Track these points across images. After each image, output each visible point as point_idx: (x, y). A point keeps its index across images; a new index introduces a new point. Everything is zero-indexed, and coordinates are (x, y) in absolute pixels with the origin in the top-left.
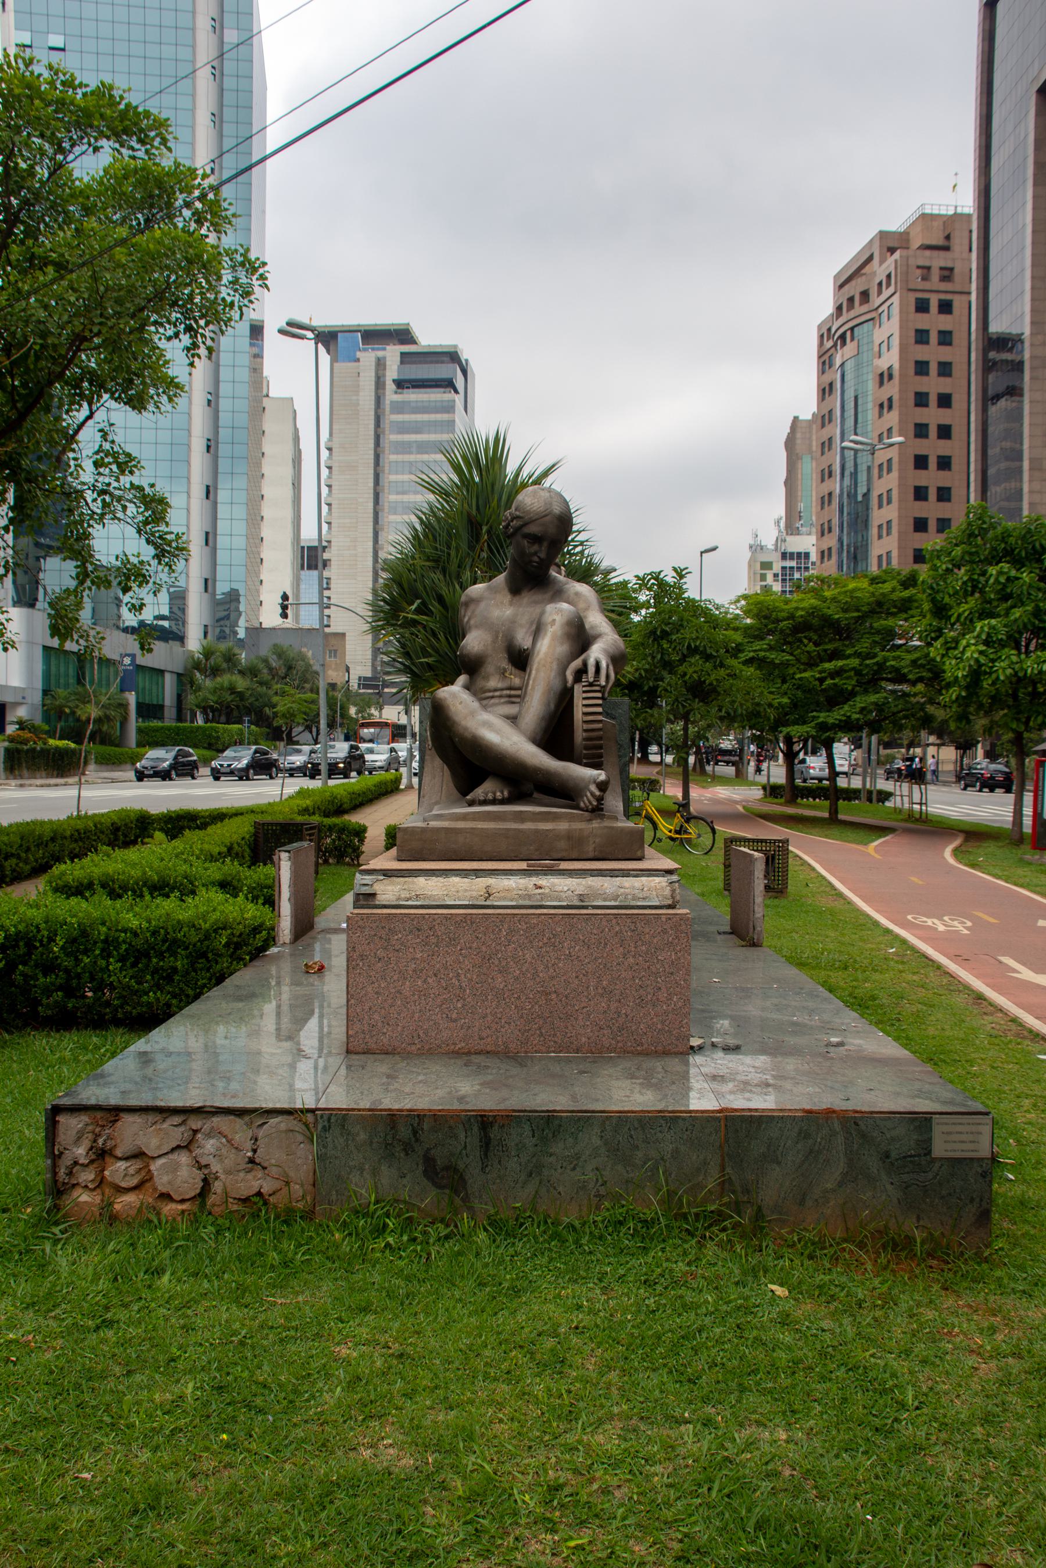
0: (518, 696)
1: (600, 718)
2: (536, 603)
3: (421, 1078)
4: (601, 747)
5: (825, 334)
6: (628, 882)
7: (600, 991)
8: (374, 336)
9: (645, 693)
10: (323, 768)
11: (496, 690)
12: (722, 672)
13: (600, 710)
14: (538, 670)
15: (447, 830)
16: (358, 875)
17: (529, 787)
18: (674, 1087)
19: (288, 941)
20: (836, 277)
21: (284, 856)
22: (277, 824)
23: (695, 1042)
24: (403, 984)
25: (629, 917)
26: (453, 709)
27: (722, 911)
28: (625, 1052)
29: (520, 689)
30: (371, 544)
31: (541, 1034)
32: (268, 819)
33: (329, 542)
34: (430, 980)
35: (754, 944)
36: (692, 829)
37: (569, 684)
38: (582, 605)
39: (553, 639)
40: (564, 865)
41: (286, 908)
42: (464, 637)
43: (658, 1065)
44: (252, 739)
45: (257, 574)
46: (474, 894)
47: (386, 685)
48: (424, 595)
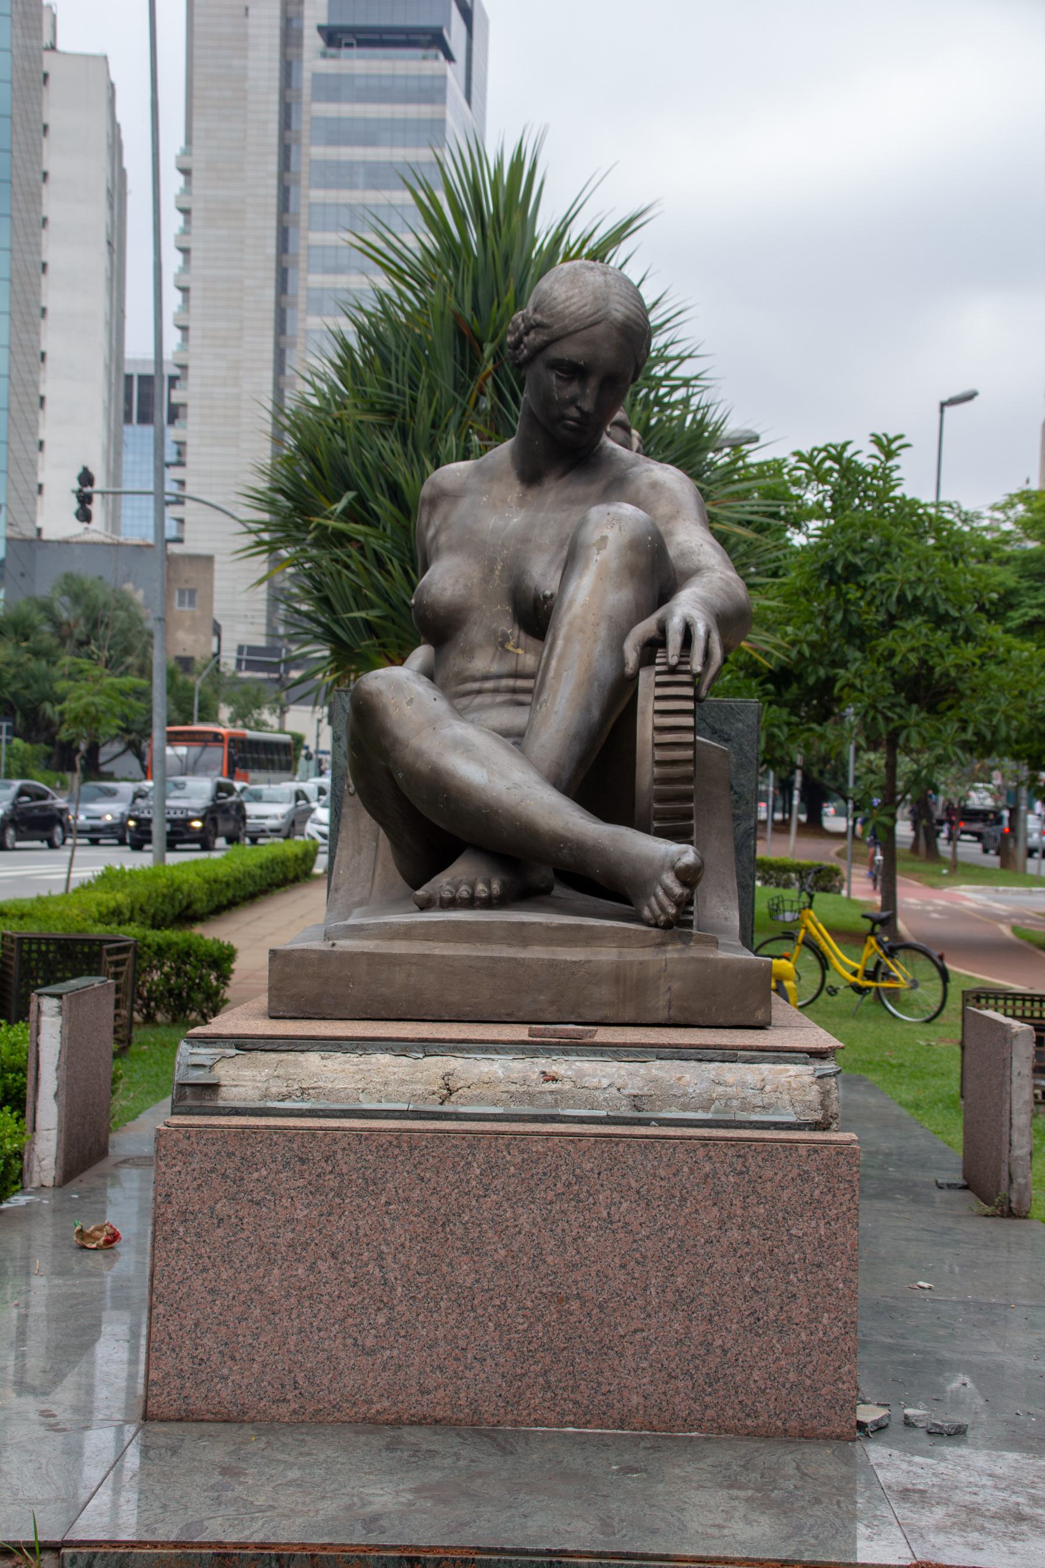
0: (528, 691)
1: (689, 737)
2: (572, 502)
3: (293, 1474)
4: (688, 797)
6: (733, 1073)
7: (670, 1297)
9: (811, 691)
10: (158, 830)
11: (486, 678)
12: (969, 651)
13: (689, 721)
14: (568, 640)
15: (371, 957)
16: (184, 1047)
17: (543, 874)
18: (818, 1510)
19: (49, 1182)
21: (49, 1005)
22: (48, 941)
23: (868, 1414)
24: (267, 1273)
25: (733, 1144)
26: (394, 713)
27: (945, 1140)
28: (722, 1430)
30: (269, 375)
31: (547, 1386)
32: (32, 929)
33: (184, 367)
34: (322, 1266)
35: (1011, 1212)
36: (900, 971)
37: (629, 669)
38: (663, 509)
39: (600, 577)
40: (603, 1035)
41: (48, 1112)
42: (426, 568)
43: (787, 1460)
44: (15, 765)
45: (33, 428)
46: (420, 1088)
47: (292, 662)
48: (363, 484)
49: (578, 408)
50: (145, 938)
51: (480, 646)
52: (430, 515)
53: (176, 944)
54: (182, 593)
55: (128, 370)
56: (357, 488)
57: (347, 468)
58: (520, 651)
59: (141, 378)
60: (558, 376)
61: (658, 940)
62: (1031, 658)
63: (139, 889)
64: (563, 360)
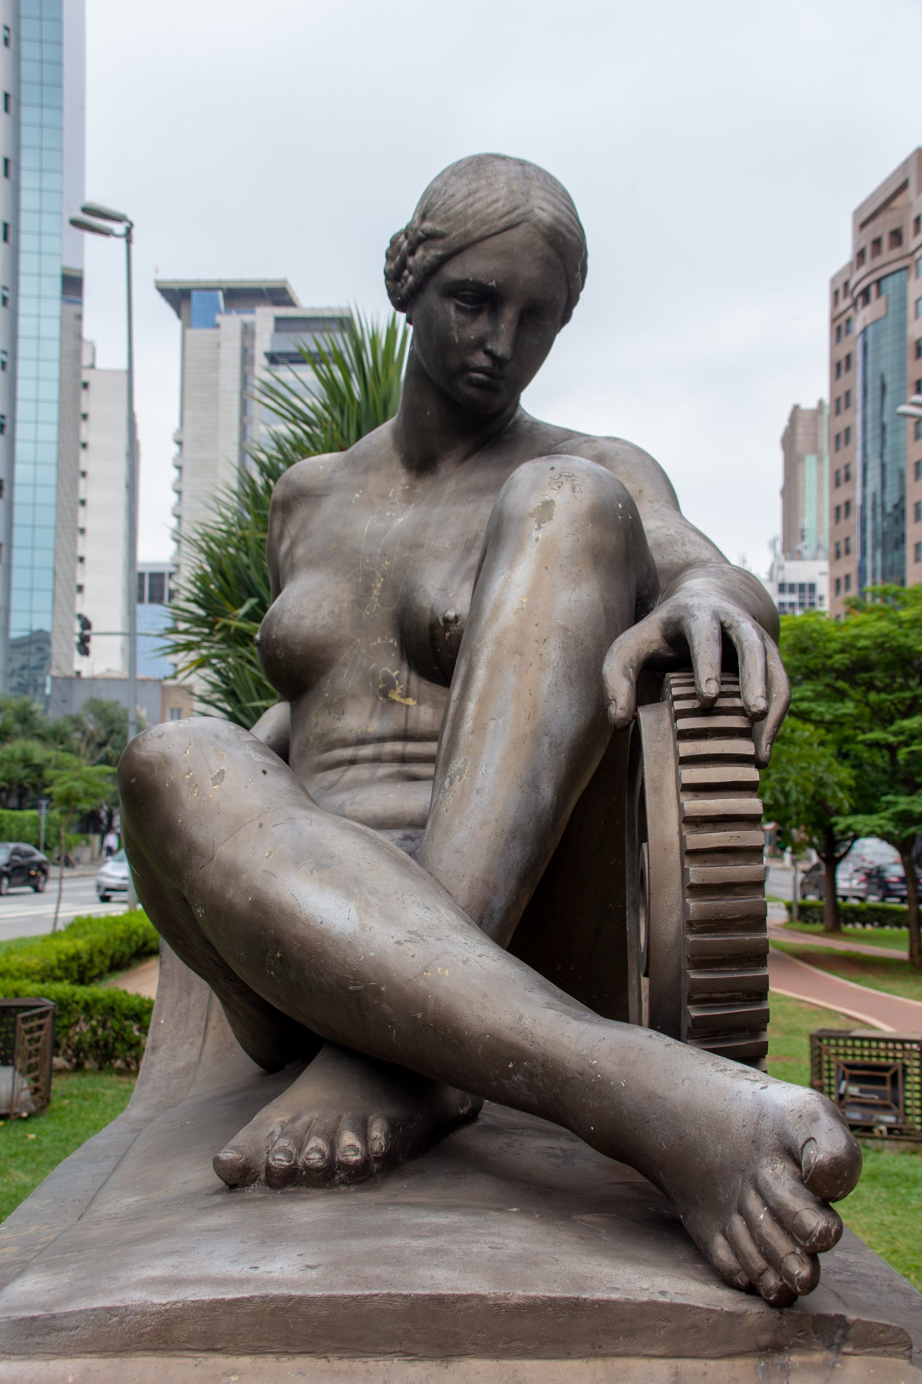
0: (430, 759)
5: (840, 290)
8: (240, 296)
11: (362, 741)
14: (495, 668)
20: (857, 213)
26: (189, 799)
29: (432, 737)
39: (544, 566)
42: (278, 591)
49: (488, 353)
50: (74, 995)
51: (354, 696)
52: (284, 523)
53: (102, 999)
54: (172, 710)
55: (140, 569)
56: (259, 595)
57: (249, 578)
58: (411, 702)
59: (153, 575)
60: (459, 309)
61: (765, 1338)
62: (811, 736)
63: (96, 936)
64: (465, 282)
